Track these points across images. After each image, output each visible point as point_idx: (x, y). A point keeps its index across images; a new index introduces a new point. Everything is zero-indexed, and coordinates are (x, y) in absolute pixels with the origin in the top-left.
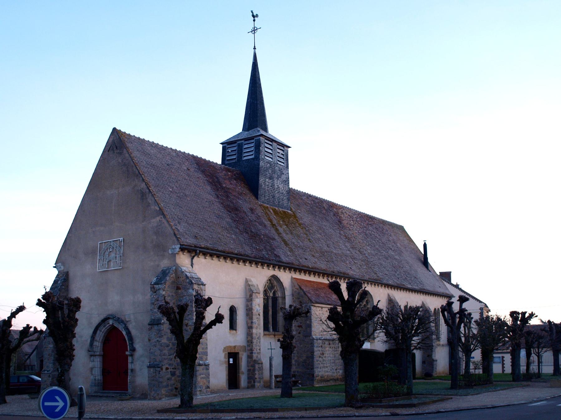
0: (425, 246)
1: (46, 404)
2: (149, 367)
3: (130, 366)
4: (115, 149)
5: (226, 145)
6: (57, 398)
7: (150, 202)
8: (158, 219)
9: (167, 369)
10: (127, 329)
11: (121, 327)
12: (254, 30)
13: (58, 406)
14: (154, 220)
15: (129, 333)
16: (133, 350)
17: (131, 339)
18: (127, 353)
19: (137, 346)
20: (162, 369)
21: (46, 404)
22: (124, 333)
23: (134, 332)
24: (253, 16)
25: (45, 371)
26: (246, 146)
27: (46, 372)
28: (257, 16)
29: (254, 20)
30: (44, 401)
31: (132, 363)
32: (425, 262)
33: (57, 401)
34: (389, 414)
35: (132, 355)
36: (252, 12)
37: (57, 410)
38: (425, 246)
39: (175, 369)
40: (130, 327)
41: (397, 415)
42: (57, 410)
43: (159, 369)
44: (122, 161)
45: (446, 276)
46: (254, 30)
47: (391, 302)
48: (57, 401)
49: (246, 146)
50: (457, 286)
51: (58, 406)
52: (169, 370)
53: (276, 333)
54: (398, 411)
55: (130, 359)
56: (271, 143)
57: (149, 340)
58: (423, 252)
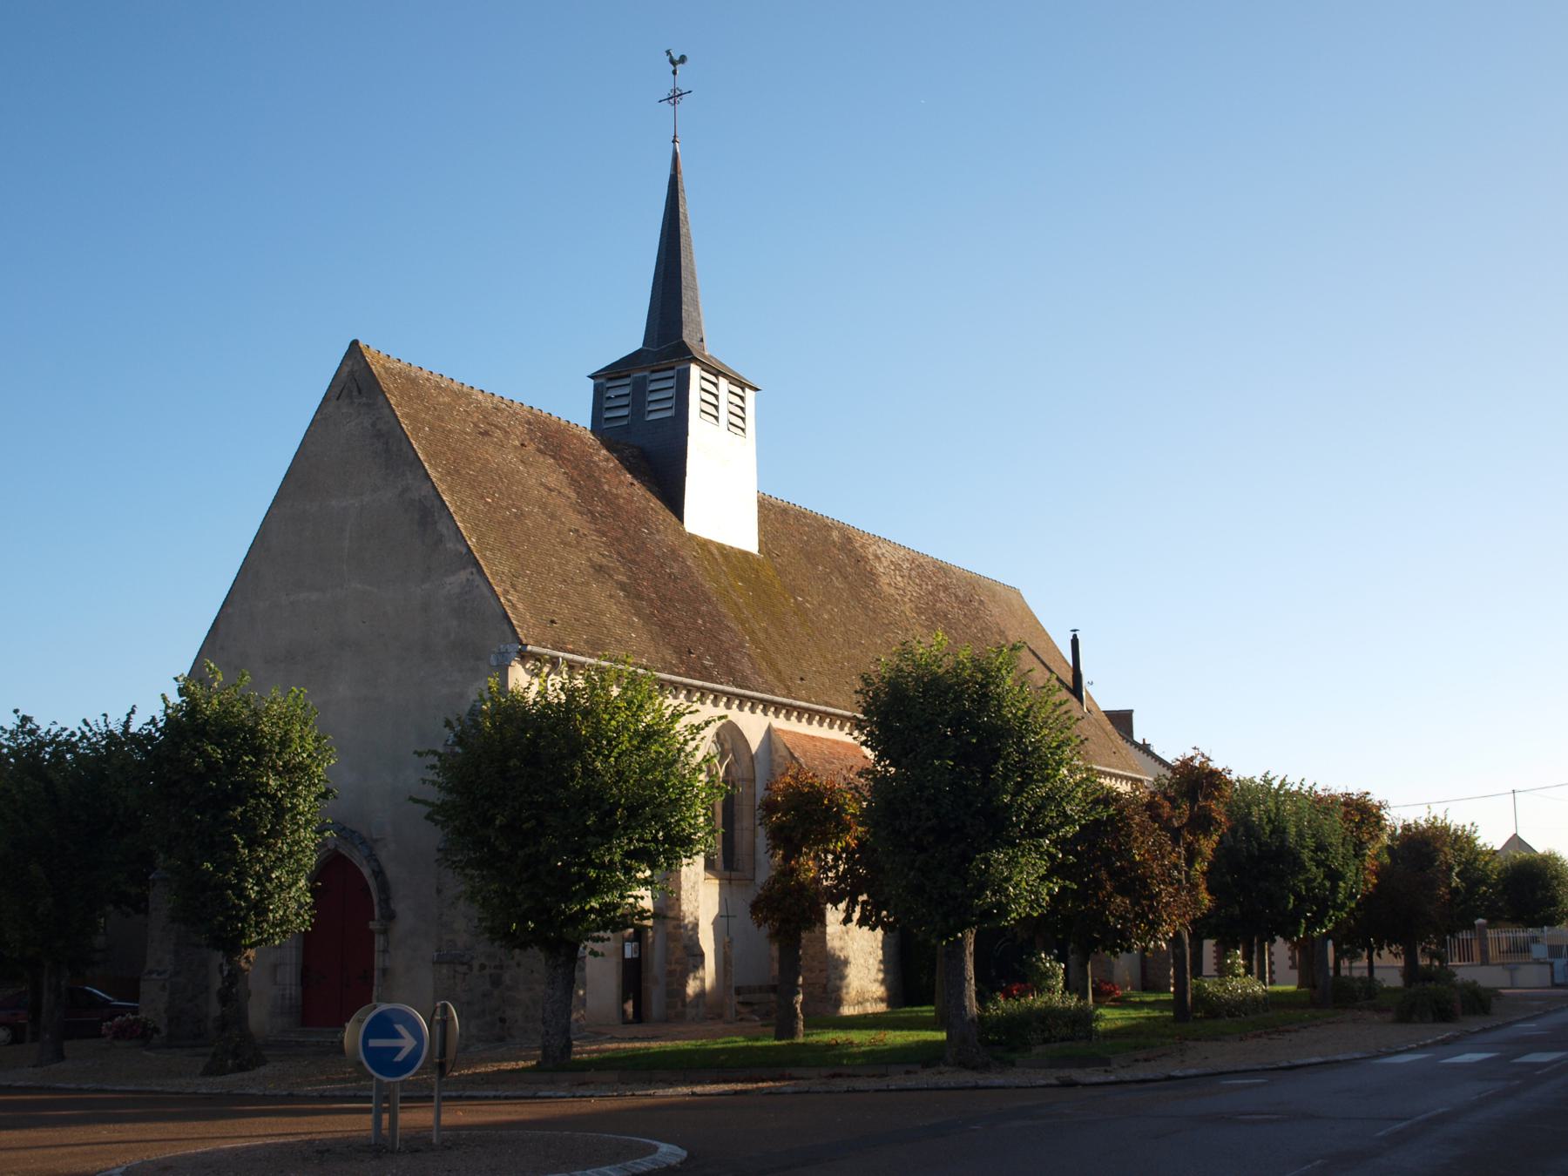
0: (1075, 643)
1: (373, 1043)
2: (439, 962)
3: (379, 961)
4: (355, 393)
5: (606, 378)
6: (400, 1028)
7: (445, 531)
8: (463, 575)
9: (483, 967)
10: (372, 857)
11: (357, 858)
12: (675, 97)
13: (399, 1049)
14: (452, 579)
15: (379, 873)
16: (390, 916)
17: (384, 887)
18: (373, 925)
19: (400, 906)
20: (471, 967)
21: (373, 1043)
22: (366, 872)
23: (391, 871)
24: (673, 62)
25: (151, 972)
26: (653, 386)
27: (154, 976)
28: (683, 59)
29: (674, 73)
30: (366, 1037)
31: (385, 951)
32: (1076, 689)
33: (397, 1035)
34: (1054, 1082)
35: (385, 932)
36: (668, 52)
37: (399, 1058)
38: (1075, 643)
39: (501, 967)
40: (383, 855)
41: (1071, 1084)
42: (399, 1058)
43: (464, 969)
44: (373, 425)
45: (1122, 721)
46: (675, 97)
47: (730, 737)
48: (397, 1035)
49: (653, 386)
50: (1145, 748)
51: (399, 1049)
52: (487, 972)
53: (734, 874)
54: (1077, 1075)
55: (379, 942)
56: (713, 378)
57: (439, 891)
58: (1070, 662)
